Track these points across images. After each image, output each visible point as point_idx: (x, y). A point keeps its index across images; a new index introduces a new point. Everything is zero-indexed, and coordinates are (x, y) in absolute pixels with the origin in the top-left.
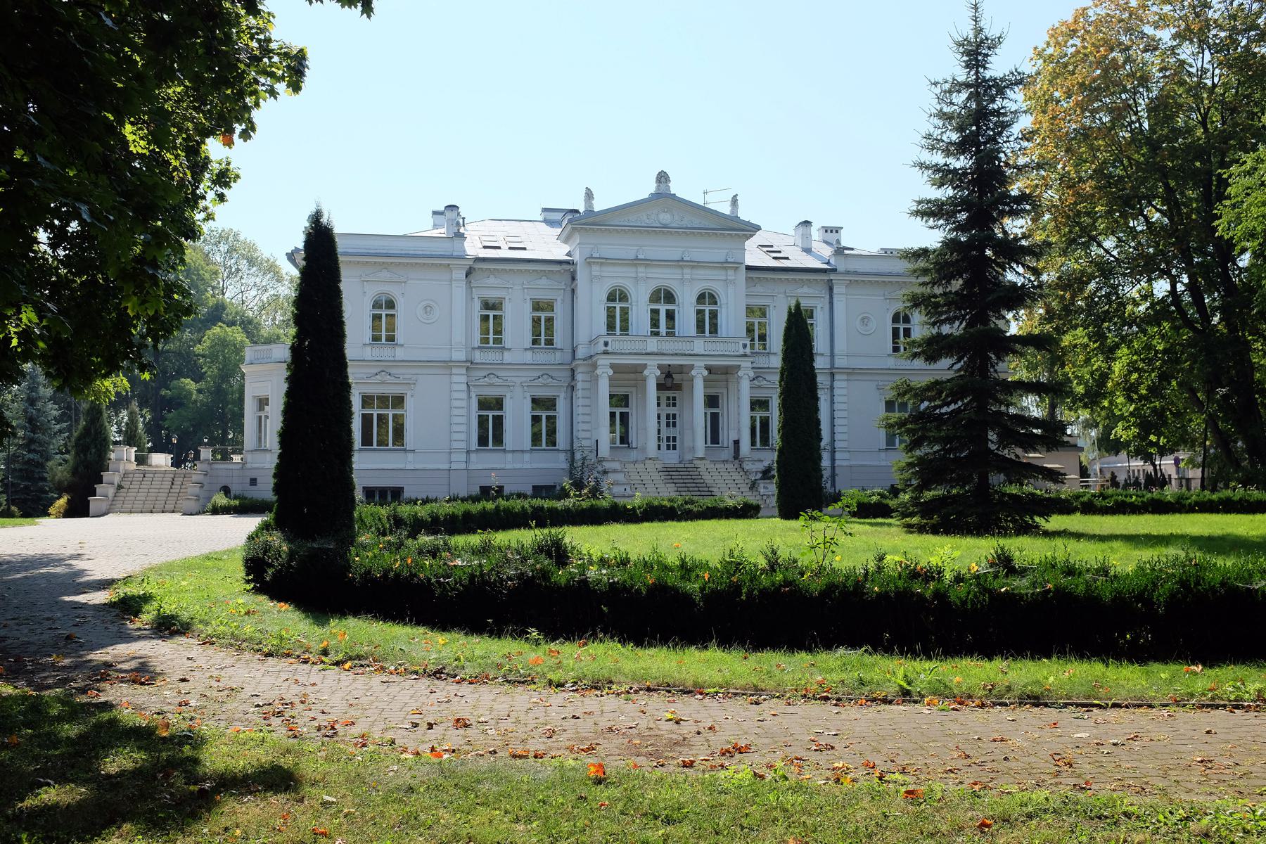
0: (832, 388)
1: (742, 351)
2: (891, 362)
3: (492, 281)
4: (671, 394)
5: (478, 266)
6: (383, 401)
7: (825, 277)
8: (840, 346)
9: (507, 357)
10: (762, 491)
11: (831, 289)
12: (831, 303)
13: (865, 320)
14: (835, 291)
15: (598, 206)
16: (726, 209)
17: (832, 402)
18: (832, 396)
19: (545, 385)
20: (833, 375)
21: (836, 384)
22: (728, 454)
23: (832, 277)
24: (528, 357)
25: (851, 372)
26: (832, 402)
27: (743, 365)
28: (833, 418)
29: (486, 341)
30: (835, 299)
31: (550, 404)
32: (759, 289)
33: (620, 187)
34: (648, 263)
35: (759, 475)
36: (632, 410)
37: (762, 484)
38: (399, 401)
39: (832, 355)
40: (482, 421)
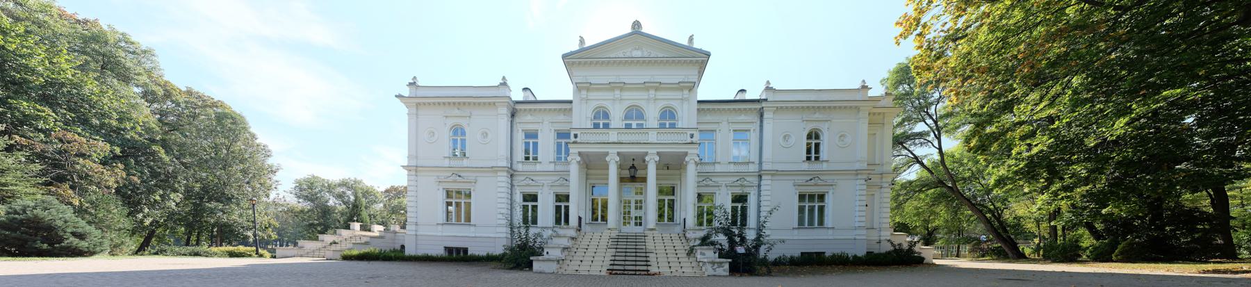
0: (759, 186)
1: (689, 140)
2: (806, 166)
3: (529, 118)
4: (638, 185)
5: (518, 107)
6: (812, 197)
7: (758, 106)
8: (767, 155)
9: (538, 167)
10: (699, 256)
11: (762, 116)
12: (761, 126)
13: (786, 137)
14: (765, 116)
15: (588, 44)
16: (685, 42)
17: (759, 195)
18: (759, 191)
19: (455, 181)
20: (760, 176)
21: (763, 183)
22: (679, 229)
23: (764, 104)
24: (551, 167)
25: (775, 174)
26: (759, 195)
27: (690, 151)
28: (759, 206)
29: (527, 158)
30: (765, 122)
31: (534, 198)
32: (709, 118)
33: (604, 27)
34: (623, 87)
35: (698, 242)
36: (676, 198)
37: (699, 250)
38: (821, 197)
39: (760, 163)
40: (558, 209)
